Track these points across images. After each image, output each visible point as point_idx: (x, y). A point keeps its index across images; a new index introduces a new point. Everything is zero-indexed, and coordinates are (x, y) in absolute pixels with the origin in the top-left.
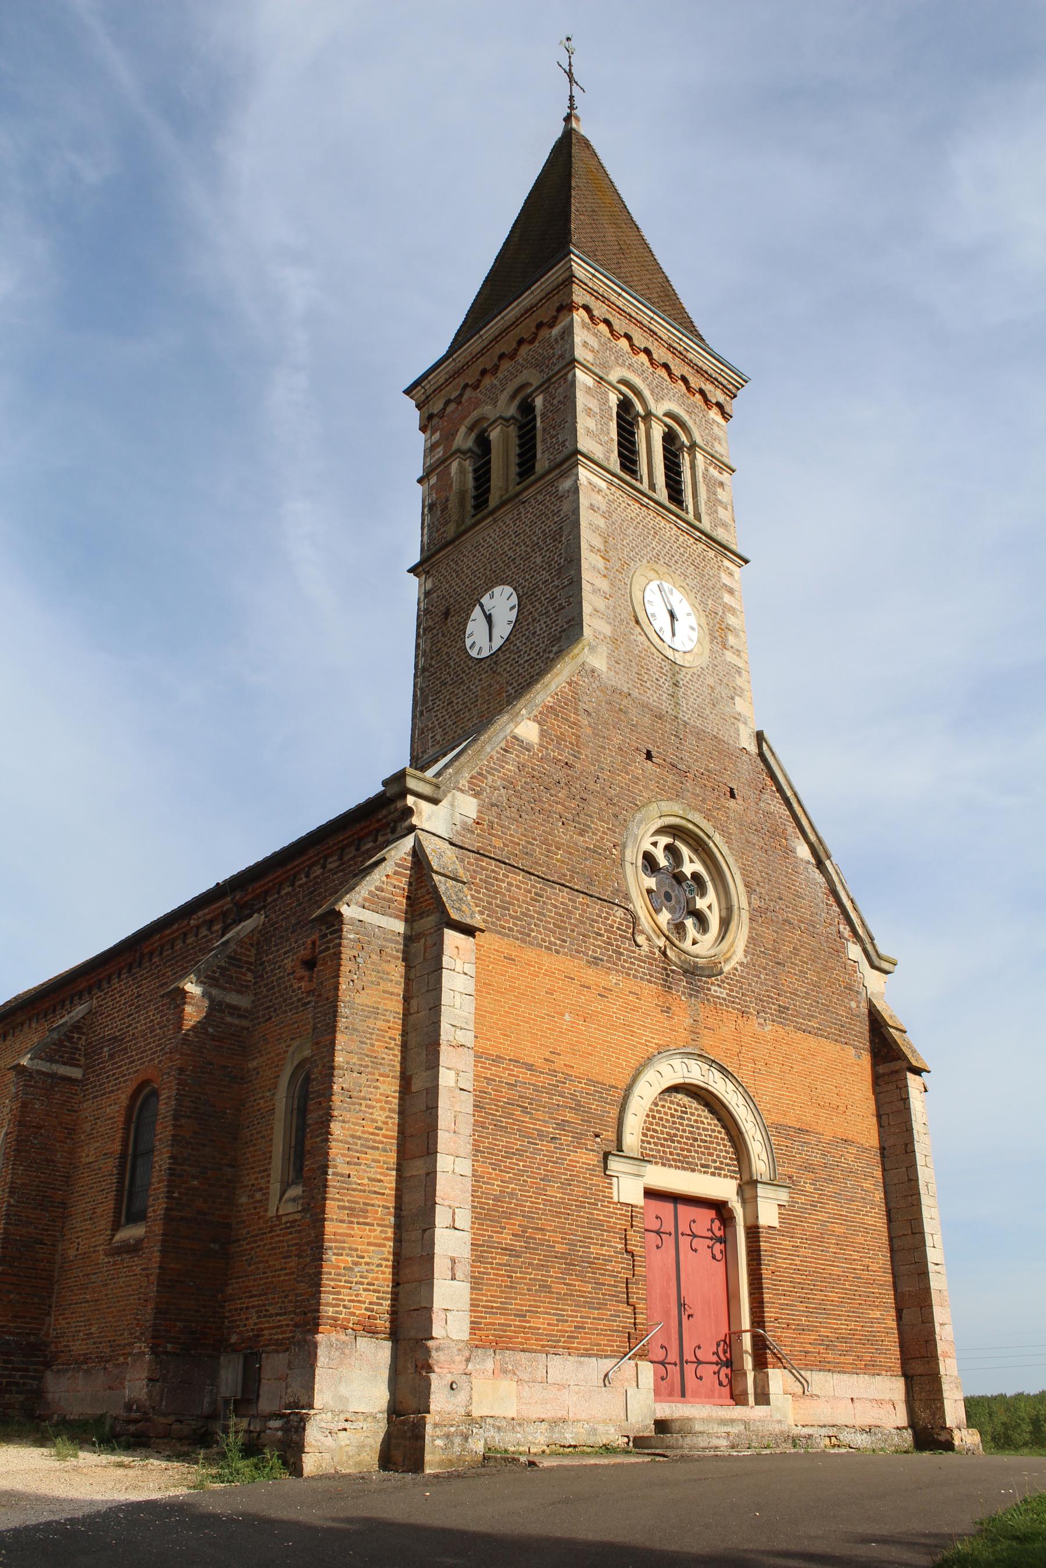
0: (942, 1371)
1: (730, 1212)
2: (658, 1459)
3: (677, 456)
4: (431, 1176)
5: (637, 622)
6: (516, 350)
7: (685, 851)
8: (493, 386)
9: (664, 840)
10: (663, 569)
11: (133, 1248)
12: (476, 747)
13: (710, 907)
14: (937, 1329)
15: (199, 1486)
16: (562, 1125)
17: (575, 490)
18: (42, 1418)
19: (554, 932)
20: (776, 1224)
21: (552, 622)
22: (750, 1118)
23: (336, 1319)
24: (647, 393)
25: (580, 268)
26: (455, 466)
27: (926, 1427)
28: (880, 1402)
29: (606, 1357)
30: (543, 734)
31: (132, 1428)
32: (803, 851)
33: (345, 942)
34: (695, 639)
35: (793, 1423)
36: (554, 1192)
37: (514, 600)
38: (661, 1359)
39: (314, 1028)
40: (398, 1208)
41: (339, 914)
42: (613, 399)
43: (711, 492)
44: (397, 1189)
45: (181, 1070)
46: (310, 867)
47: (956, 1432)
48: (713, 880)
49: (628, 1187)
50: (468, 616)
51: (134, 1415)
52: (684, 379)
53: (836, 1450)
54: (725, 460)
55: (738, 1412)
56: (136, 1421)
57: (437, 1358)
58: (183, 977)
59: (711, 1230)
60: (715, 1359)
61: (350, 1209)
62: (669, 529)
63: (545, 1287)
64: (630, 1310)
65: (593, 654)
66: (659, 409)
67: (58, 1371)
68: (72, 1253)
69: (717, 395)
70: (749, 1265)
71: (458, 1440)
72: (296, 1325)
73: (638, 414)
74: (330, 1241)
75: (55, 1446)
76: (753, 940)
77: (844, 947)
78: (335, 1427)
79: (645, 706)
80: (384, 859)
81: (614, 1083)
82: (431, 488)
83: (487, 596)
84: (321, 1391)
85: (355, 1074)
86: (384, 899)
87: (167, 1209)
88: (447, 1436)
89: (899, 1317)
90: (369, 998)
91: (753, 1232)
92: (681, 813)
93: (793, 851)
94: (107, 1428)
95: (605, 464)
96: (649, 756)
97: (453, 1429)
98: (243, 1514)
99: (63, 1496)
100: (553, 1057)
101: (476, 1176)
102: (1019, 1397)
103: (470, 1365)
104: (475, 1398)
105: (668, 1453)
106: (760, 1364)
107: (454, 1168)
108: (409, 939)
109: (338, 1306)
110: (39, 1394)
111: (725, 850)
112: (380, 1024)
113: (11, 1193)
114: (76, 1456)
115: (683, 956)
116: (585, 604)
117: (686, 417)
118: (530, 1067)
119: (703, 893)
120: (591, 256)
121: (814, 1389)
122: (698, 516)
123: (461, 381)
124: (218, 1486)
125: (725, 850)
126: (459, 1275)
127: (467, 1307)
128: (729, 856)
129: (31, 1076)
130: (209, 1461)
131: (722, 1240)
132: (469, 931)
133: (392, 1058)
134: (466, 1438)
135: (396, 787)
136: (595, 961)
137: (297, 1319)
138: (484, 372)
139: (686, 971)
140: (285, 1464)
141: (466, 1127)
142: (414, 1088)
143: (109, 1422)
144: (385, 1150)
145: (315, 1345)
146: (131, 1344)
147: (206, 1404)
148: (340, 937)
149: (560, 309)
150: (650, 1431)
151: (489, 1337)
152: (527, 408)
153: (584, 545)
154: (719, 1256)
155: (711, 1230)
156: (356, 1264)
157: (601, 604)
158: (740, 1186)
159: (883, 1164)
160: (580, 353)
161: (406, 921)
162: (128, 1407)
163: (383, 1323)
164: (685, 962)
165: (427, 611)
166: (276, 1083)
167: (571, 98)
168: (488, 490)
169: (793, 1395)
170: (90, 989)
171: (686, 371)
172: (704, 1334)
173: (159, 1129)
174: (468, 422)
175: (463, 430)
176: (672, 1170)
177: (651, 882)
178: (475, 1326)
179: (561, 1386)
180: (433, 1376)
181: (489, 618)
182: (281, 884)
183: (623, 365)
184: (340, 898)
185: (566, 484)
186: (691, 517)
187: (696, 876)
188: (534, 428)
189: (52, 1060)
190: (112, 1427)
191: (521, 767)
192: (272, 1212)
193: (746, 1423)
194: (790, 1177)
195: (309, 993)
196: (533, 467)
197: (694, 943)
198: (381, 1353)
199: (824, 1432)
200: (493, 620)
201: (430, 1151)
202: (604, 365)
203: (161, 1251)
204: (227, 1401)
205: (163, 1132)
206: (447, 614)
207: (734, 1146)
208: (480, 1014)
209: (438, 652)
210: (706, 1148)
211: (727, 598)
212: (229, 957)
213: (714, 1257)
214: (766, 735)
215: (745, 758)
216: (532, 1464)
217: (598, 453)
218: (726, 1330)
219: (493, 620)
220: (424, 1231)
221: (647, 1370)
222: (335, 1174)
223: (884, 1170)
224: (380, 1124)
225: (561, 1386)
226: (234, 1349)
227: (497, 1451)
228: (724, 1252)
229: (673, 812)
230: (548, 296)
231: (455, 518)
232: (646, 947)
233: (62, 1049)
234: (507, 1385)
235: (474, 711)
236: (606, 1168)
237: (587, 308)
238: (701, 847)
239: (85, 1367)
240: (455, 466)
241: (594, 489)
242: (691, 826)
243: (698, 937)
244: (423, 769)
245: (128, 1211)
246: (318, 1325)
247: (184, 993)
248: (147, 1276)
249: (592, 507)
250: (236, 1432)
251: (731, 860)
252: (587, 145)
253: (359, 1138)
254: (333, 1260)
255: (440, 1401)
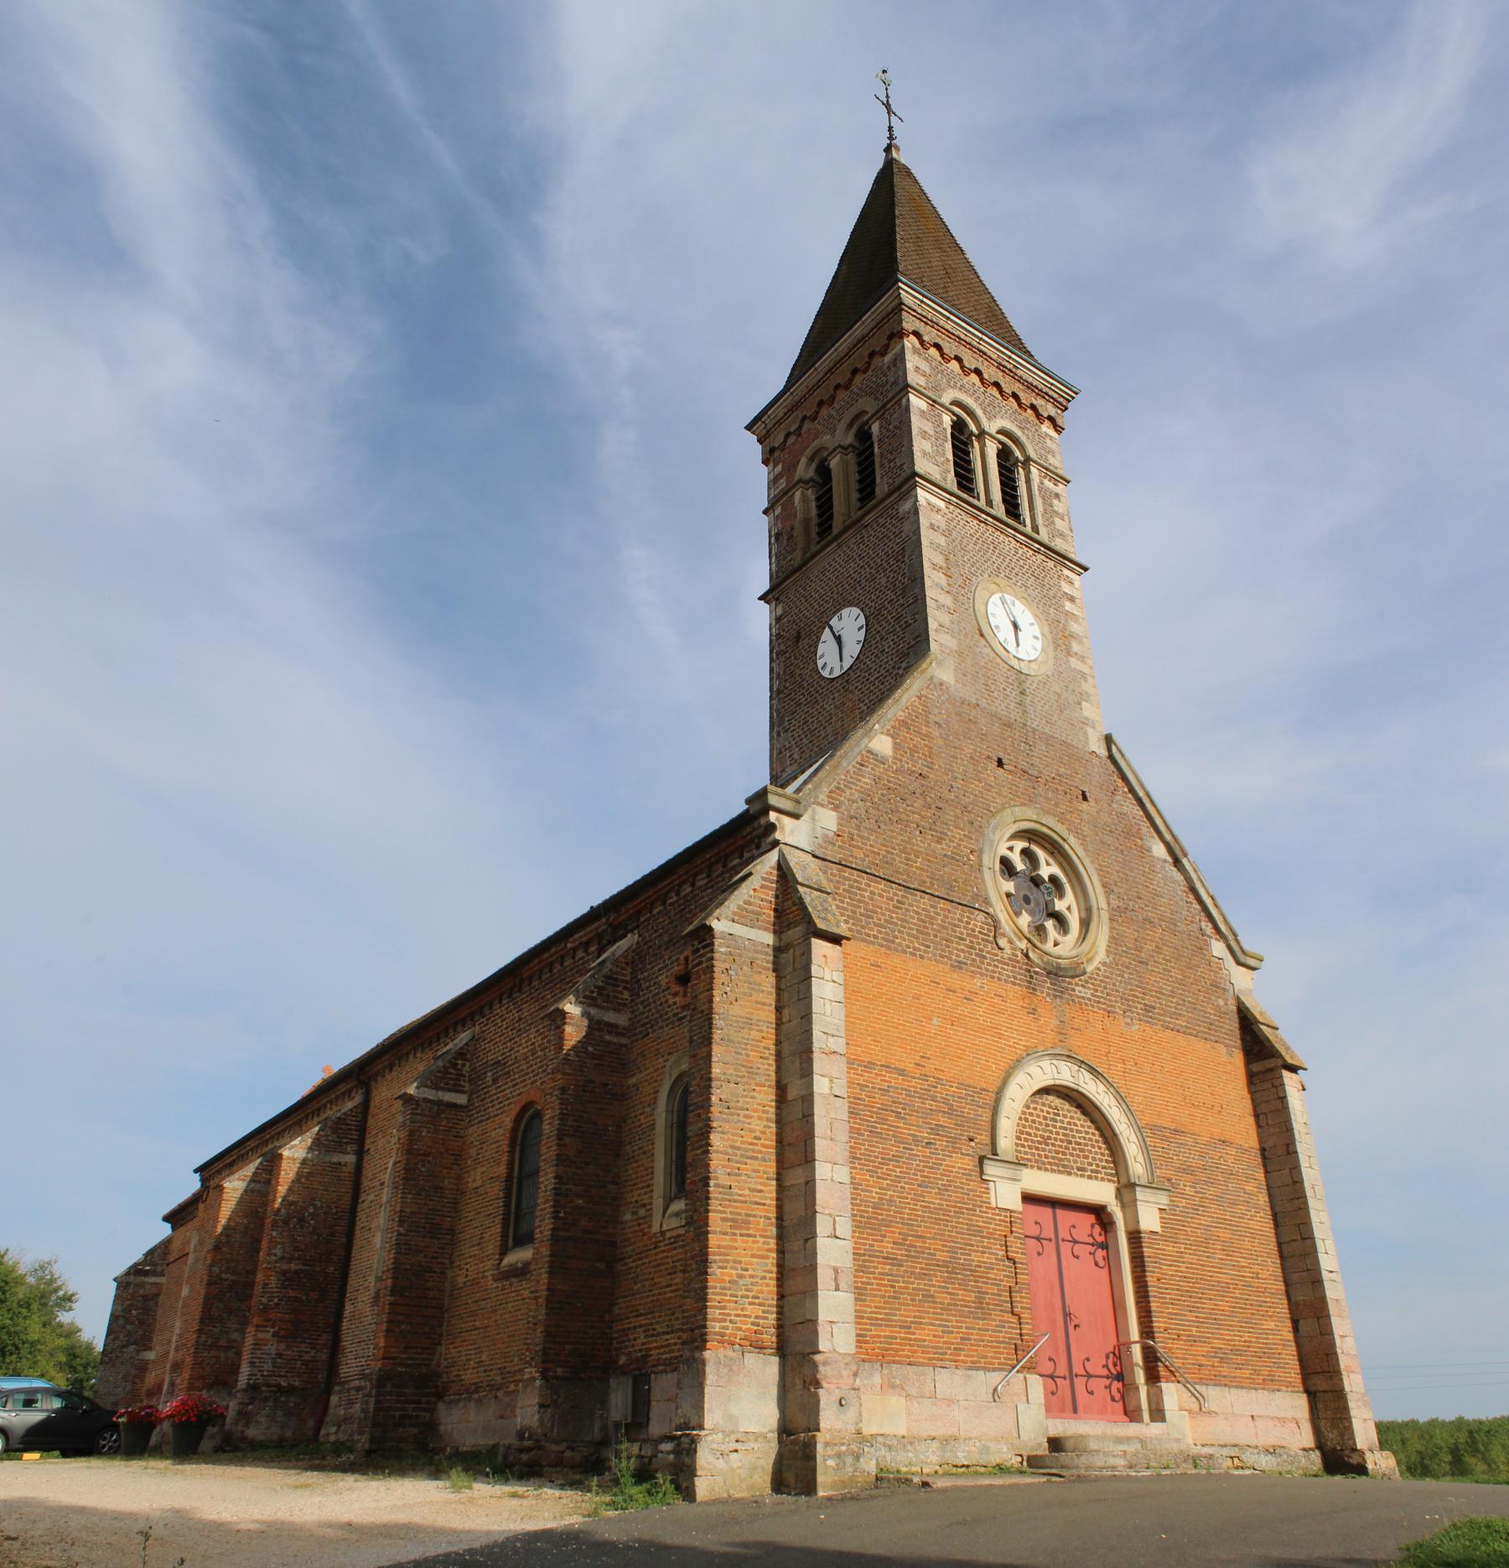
0: (1347, 1388)
1: (1110, 1216)
2: (1054, 1479)
3: (1012, 472)
4: (810, 1183)
5: (982, 635)
6: (851, 380)
7: (1041, 855)
8: (830, 416)
9: (1020, 845)
10: (1003, 582)
11: (521, 1272)
12: (833, 762)
13: (1069, 908)
14: (1338, 1341)
15: (594, 1513)
16: (935, 1130)
17: (916, 511)
18: (435, 1451)
19: (917, 938)
20: (1158, 1229)
21: (900, 641)
22: (1124, 1119)
23: (722, 1335)
24: (979, 412)
25: (908, 296)
26: (798, 495)
27: (1335, 1449)
28: (1283, 1421)
29: (994, 1370)
30: (896, 747)
31: (524, 1457)
32: (1159, 850)
33: (716, 956)
34: (1039, 648)
35: (1191, 1442)
36: (932, 1198)
37: (862, 621)
38: (1049, 1372)
39: (691, 1042)
40: (780, 1218)
41: (710, 929)
42: (947, 420)
43: (1048, 504)
44: (778, 1199)
45: (563, 1090)
46: (680, 885)
47: (1368, 1455)
48: (1070, 881)
49: (1006, 1193)
50: (819, 638)
51: (527, 1443)
52: (1015, 396)
53: (1240, 1472)
54: (1059, 471)
55: (1132, 1429)
56: (528, 1450)
57: (824, 1372)
58: (560, 999)
59: (1091, 1235)
60: (1105, 1372)
61: (732, 1220)
62: (1008, 543)
63: (928, 1297)
64: (1015, 1319)
65: (941, 667)
66: (992, 427)
67: (451, 1402)
68: (461, 1280)
69: (1049, 409)
70: (1133, 1272)
71: (849, 1460)
72: (684, 1343)
73: (972, 434)
74: (715, 1254)
75: (449, 1477)
76: (1114, 940)
77: (1207, 944)
78: (726, 1448)
79: (993, 715)
80: (750, 874)
81: (984, 1086)
82: (776, 518)
83: (836, 618)
84: (710, 1410)
85: (732, 1085)
86: (753, 912)
87: (553, 1230)
88: (839, 1455)
89: (1296, 1329)
90: (741, 1006)
91: (1135, 1237)
92: (1034, 817)
93: (1149, 850)
94: (500, 1457)
95: (942, 484)
96: (1000, 763)
97: (844, 1448)
98: (639, 1541)
99: (460, 1527)
100: (924, 1062)
101: (854, 1183)
102: (1433, 1423)
103: (858, 1381)
104: (865, 1415)
105: (1064, 1472)
106: (1153, 1377)
107: (832, 1175)
108: (778, 950)
109: (724, 1321)
110: (431, 1426)
111: (1081, 852)
112: (754, 1034)
113: (401, 1222)
114: (470, 1488)
115: (1046, 958)
116: (930, 620)
117: (1018, 433)
118: (901, 1072)
119: (1061, 896)
120: (919, 282)
121: (1210, 1405)
122: (1035, 529)
123: (799, 414)
124: (612, 1513)
125: (1081, 852)
126: (843, 1285)
127: (852, 1319)
128: (1081, 842)
129: (418, 1104)
130: (603, 1488)
131: (1104, 1246)
132: (836, 939)
133: (768, 1068)
134: (858, 1458)
135: (759, 803)
136: (959, 965)
137: (685, 1336)
138: (821, 404)
139: (1049, 973)
140: (678, 1488)
141: (842, 1135)
142: (790, 1097)
143: (501, 1450)
144: (764, 1160)
145: (703, 1363)
146: (521, 1371)
147: (596, 1430)
148: (712, 951)
149: (891, 337)
150: (1043, 1450)
151: (875, 1351)
152: (864, 436)
153: (926, 564)
154: (1101, 1263)
155: (1091, 1235)
156: (741, 1277)
157: (945, 619)
158: (1118, 1190)
159: (1265, 1166)
160: (913, 378)
161: (775, 932)
162: (520, 1435)
163: (770, 1337)
164: (1047, 963)
165: (778, 636)
166: (655, 1099)
167: (890, 129)
168: (831, 517)
169: (1190, 1411)
170: (472, 1017)
171: (1017, 388)
172: (1092, 1346)
173: (543, 1149)
174: (808, 452)
175: (804, 460)
176: (1048, 1174)
177: (1009, 886)
178: (861, 1340)
179: (950, 1401)
180: (821, 1392)
181: (838, 639)
182: (652, 904)
183: (954, 387)
184: (710, 914)
185: (906, 506)
186: (1028, 530)
187: (1053, 879)
188: (872, 454)
189: (437, 1088)
190: (505, 1457)
191: (877, 780)
192: (656, 1228)
193: (1142, 1441)
194: (1169, 1180)
195: (684, 1007)
196: (873, 492)
197: (1056, 944)
198: (768, 1369)
199: (1225, 1452)
200: (843, 639)
201: (809, 1159)
202: (936, 389)
203: (549, 1273)
204: (617, 1425)
205: (547, 1151)
206: (798, 638)
207: (1109, 1148)
208: (850, 1021)
209: (792, 674)
210: (1082, 1150)
211: (1068, 606)
212: (606, 977)
213: (1096, 1264)
214: (1115, 737)
215: (1095, 761)
216: (925, 1484)
217: (934, 472)
218: (1113, 1341)
219: (843, 639)
220: (806, 1241)
221: (1036, 1385)
222: (716, 1186)
223: (1266, 1172)
224: (758, 1134)
225: (950, 1401)
226: (623, 1371)
227: (888, 1471)
228: (1107, 1259)
229: (1028, 816)
230: (879, 325)
231: (800, 545)
232: (1008, 951)
233: (446, 1077)
234: (896, 1402)
235: (829, 729)
236: (982, 1172)
237: (917, 334)
238: (1056, 850)
239: (476, 1396)
240: (798, 495)
241: (933, 508)
242: (1045, 830)
243: (1060, 938)
244: (783, 786)
245: (516, 1233)
246: (706, 1341)
247: (563, 1014)
248: (536, 1298)
249: (932, 527)
250: (629, 1458)
251: (1087, 861)
252: (908, 173)
253: (739, 1148)
254: (718, 1274)
255: (830, 1419)
